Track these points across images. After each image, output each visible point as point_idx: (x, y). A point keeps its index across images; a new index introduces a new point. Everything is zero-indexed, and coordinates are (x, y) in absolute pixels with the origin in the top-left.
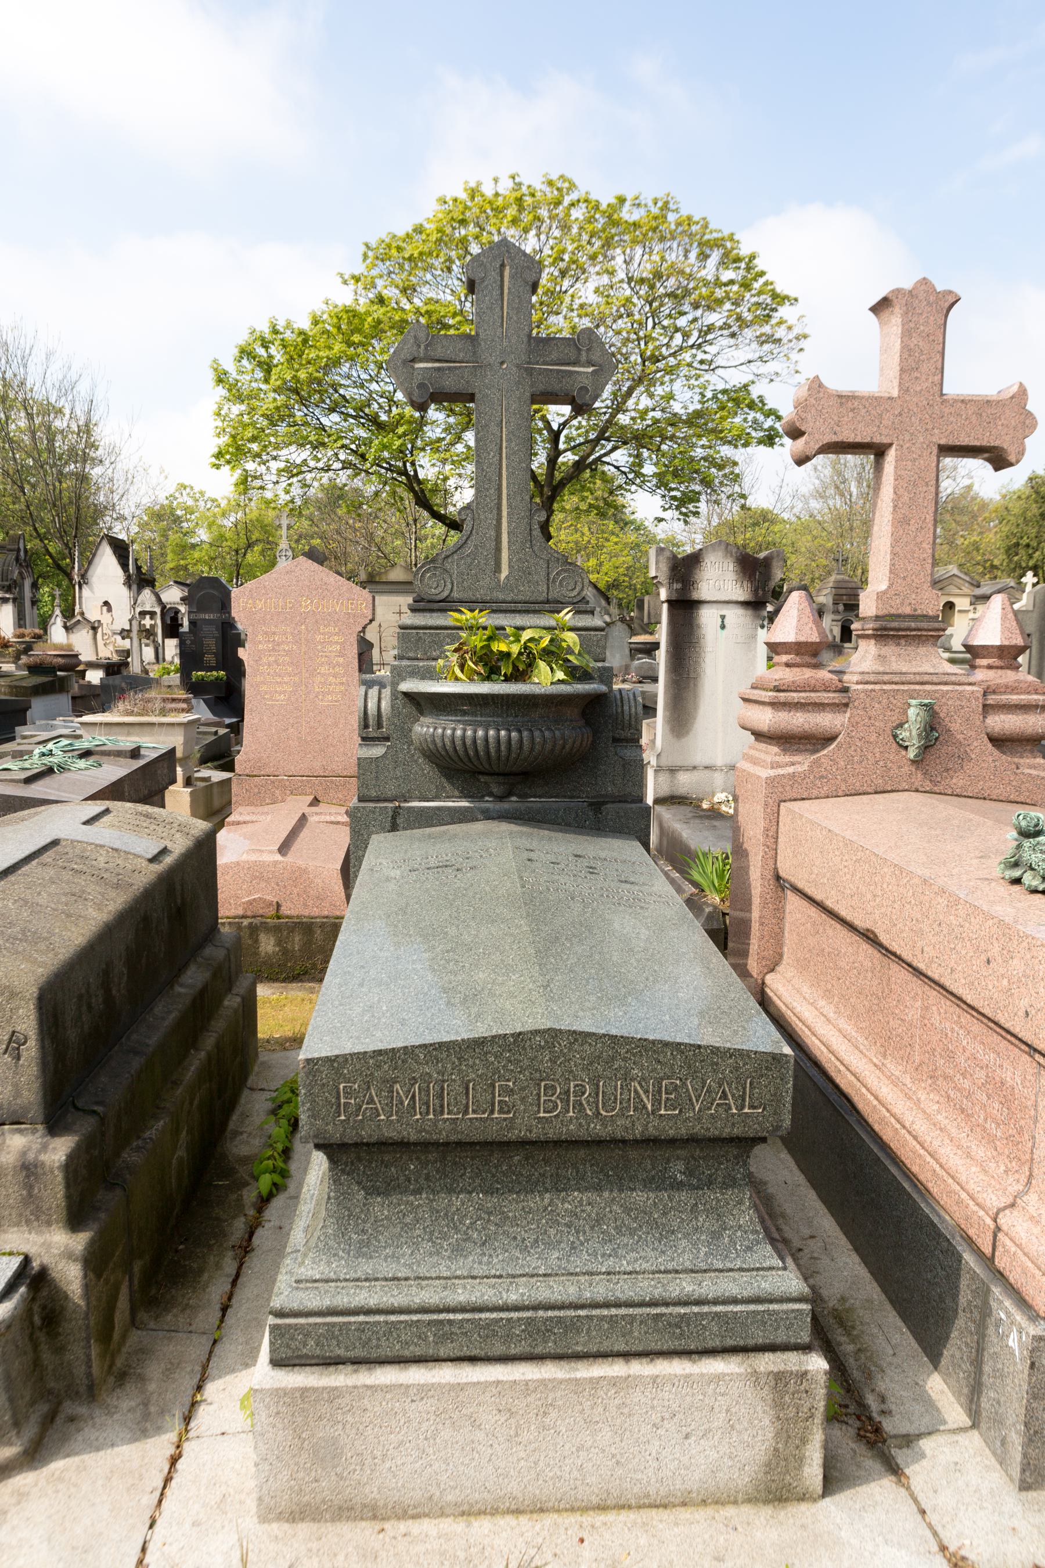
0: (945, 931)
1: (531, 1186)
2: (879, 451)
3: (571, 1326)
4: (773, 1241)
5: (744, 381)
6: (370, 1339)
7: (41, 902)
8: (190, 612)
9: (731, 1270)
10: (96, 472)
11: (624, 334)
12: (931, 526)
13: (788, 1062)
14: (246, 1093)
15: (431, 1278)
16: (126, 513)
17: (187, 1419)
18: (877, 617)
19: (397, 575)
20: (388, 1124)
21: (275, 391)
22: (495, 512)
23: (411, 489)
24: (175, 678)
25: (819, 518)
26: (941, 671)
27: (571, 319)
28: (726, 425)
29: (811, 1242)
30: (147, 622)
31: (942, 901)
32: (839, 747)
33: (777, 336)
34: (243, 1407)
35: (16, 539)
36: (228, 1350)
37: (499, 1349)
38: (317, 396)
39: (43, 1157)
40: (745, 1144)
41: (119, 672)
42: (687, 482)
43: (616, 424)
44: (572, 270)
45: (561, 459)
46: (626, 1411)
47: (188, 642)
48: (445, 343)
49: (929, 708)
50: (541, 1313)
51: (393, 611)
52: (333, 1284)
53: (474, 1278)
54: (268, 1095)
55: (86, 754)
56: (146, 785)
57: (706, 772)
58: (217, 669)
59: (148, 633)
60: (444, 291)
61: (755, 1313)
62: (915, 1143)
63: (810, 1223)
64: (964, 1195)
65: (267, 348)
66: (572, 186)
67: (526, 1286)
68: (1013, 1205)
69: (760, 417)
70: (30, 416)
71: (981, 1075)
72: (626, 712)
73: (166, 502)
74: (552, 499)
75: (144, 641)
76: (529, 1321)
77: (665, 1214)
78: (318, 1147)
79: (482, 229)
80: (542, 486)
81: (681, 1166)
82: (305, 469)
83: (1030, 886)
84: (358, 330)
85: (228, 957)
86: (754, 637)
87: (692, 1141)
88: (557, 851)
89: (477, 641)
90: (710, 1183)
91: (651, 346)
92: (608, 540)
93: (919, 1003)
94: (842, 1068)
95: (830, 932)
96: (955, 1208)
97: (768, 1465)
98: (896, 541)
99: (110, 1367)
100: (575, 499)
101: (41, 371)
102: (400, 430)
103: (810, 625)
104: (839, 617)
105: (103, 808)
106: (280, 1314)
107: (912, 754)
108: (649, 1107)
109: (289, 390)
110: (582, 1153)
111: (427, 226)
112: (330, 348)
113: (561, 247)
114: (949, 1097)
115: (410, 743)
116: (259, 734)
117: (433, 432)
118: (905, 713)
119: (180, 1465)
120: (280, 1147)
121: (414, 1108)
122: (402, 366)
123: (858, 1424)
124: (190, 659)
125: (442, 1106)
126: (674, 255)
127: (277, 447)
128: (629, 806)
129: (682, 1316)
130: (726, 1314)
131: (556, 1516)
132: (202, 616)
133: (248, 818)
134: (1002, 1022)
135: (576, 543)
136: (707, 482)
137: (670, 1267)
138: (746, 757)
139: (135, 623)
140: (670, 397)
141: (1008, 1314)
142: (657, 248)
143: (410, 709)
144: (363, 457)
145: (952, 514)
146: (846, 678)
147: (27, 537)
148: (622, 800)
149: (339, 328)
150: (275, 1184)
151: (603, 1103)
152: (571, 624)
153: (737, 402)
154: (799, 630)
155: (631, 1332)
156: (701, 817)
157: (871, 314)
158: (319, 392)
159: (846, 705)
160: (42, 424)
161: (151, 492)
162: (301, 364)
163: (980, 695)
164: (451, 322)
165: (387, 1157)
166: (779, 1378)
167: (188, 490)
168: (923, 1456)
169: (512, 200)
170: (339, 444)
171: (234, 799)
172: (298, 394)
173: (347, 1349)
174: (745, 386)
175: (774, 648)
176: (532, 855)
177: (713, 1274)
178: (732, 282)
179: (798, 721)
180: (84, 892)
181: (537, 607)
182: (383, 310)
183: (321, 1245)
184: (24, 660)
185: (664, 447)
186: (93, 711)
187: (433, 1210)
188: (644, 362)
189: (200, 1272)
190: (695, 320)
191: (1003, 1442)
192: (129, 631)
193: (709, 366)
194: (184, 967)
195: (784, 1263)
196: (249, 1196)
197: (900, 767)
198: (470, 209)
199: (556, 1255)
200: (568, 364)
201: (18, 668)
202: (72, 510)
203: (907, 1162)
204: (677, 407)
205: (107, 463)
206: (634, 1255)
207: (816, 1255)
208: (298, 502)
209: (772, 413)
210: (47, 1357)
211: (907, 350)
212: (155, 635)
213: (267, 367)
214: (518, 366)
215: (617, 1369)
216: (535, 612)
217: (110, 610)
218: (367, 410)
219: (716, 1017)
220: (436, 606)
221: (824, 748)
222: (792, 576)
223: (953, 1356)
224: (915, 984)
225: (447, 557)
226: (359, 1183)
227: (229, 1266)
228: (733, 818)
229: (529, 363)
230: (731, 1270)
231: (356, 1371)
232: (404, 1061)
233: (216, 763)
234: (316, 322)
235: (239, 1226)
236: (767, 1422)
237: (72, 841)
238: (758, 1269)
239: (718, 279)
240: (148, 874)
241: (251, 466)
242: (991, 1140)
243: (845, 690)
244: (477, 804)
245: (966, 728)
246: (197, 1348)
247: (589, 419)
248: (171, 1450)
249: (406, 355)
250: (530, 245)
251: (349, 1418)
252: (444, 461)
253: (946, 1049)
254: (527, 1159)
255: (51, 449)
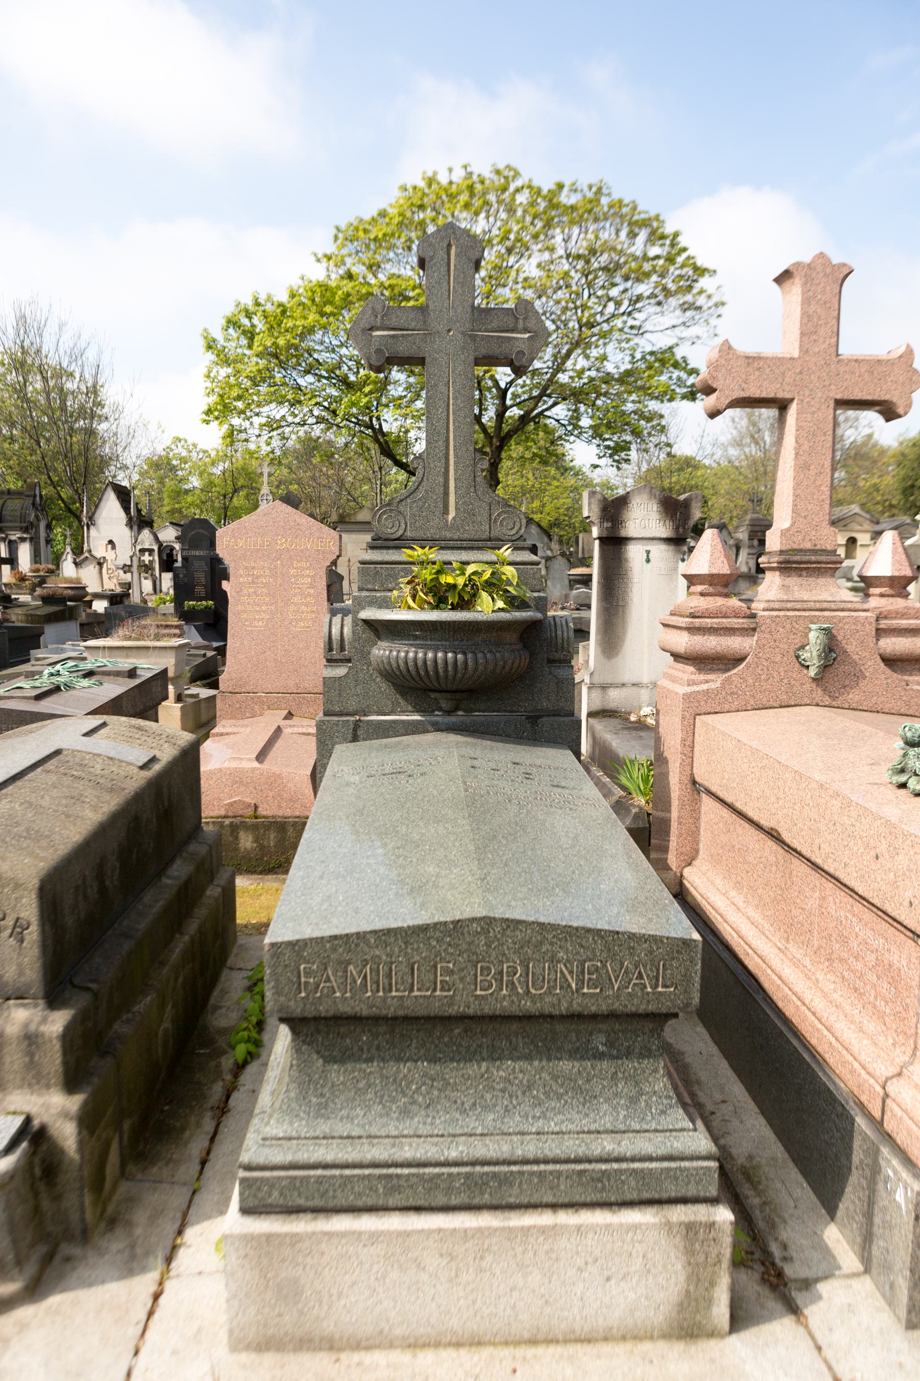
0: (839, 830)
1: (470, 1056)
2: (782, 406)
3: (505, 1180)
4: (684, 1106)
5: (669, 344)
6: (327, 1191)
7: (44, 804)
8: (182, 550)
9: (647, 1131)
10: (102, 427)
11: (563, 303)
12: (828, 471)
13: (696, 946)
14: (226, 972)
15: (380, 1137)
16: (128, 462)
17: (169, 1260)
18: (781, 551)
19: (364, 516)
20: (343, 1001)
21: (257, 356)
22: (443, 461)
23: (377, 441)
24: (170, 607)
25: (737, 464)
26: (838, 599)
27: (516, 291)
28: (654, 382)
29: (723, 1106)
30: (146, 558)
31: (837, 803)
32: (748, 667)
33: (698, 304)
34: (217, 1249)
35: (33, 486)
36: (205, 1199)
37: (441, 1200)
38: (294, 360)
39: (43, 1028)
40: (660, 1018)
41: (121, 602)
42: (619, 432)
43: (557, 382)
44: (517, 248)
45: (508, 414)
46: (554, 1256)
47: (181, 576)
48: (399, 313)
49: (828, 632)
50: (478, 1169)
51: (356, 547)
52: (295, 1142)
53: (419, 1136)
54: (245, 974)
55: (89, 674)
56: (141, 701)
57: (634, 688)
58: (206, 599)
59: (147, 568)
60: (403, 268)
61: (669, 1170)
62: (813, 1018)
63: (722, 1089)
64: (856, 1065)
65: (250, 318)
66: (517, 174)
67: (465, 1144)
68: (899, 1074)
69: (683, 375)
70: (45, 379)
71: (871, 958)
72: (560, 636)
73: (164, 453)
74: (500, 448)
75: (143, 575)
76: (468, 1176)
77: (588, 1081)
78: (282, 1020)
79: (438, 213)
80: (491, 438)
81: (602, 1038)
82: (284, 423)
83: (914, 790)
84: (331, 303)
85: (210, 852)
86: (676, 569)
87: (612, 1016)
88: (497, 758)
89: (427, 574)
90: (628, 1054)
91: (586, 314)
92: (549, 484)
93: (817, 894)
94: (750, 951)
95: (740, 831)
96: (849, 1076)
97: (681, 1304)
98: (797, 485)
99: (103, 1213)
100: (521, 449)
101: (54, 340)
102: (367, 389)
103: (722, 558)
104: (754, 551)
105: (100, 722)
106: (248, 1168)
107: (812, 672)
108: (574, 986)
109: (269, 354)
110: (515, 1026)
111: (390, 210)
112: (305, 318)
113: (508, 227)
114: (843, 977)
115: (369, 664)
116: (241, 656)
117: (396, 391)
118: (806, 636)
119: (162, 1300)
120: (254, 1020)
121: (366, 985)
122: (361, 332)
123: (762, 1269)
124: (182, 591)
125: (390, 985)
126: (606, 235)
127: (259, 405)
128: (562, 719)
129: (603, 1172)
130: (642, 1170)
131: (491, 1349)
132: (193, 553)
133: (230, 730)
134: (889, 911)
135: (522, 487)
136: (636, 433)
137: (593, 1127)
138: (666, 676)
139: (135, 559)
140: (604, 358)
141: (895, 1172)
142: (592, 227)
143: (368, 634)
144: (334, 412)
145: (855, 459)
146: (754, 605)
147: (42, 484)
148: (556, 714)
149: (313, 300)
150: (249, 1053)
151: (533, 983)
152: (511, 559)
153: (663, 362)
154: (712, 563)
155: (558, 1185)
156: (629, 728)
157: (775, 285)
158: (296, 356)
159: (754, 630)
160: (55, 386)
161: (150, 445)
162: (280, 332)
163: (873, 620)
164: (411, 294)
165: (342, 1030)
166: (690, 1228)
167: (183, 442)
168: (820, 1297)
169: (464, 187)
170: (313, 401)
171: (218, 714)
172: (277, 358)
173: (307, 1199)
174: (671, 348)
175: (692, 580)
176: (475, 763)
177: (631, 1135)
178: (657, 257)
179: (711, 644)
180: (82, 795)
181: (480, 544)
182: (351, 284)
183: (285, 1107)
184: (39, 591)
185: (599, 402)
186: (96, 636)
187: (382, 1076)
188: (581, 328)
189: (183, 1129)
190: (625, 291)
191: (892, 1286)
192: (130, 566)
193: (638, 330)
194: (172, 860)
195: (694, 1124)
196: (227, 1063)
197: (802, 684)
198: (428, 195)
199: (491, 1117)
200: (507, 331)
201: (34, 599)
202: (81, 461)
203: (807, 1035)
204: (610, 367)
205: (112, 419)
206: (561, 1117)
207: (727, 1118)
208: (278, 453)
209: (694, 372)
210: (46, 1204)
211: (806, 317)
212: (153, 569)
213: (250, 335)
214: (463, 333)
215: (545, 1218)
216: (479, 548)
217: (114, 547)
218: (338, 372)
219: (634, 906)
220: (391, 543)
221: (734, 668)
222: (712, 514)
223: (847, 1209)
224: (814, 876)
225: (401, 501)
226: (318, 1052)
227: (208, 1125)
228: (655, 729)
229: (472, 330)
230: (647, 1131)
231: (315, 1219)
232: (357, 945)
233: (204, 682)
234: (293, 296)
235: (217, 1090)
236: (679, 1266)
237: (73, 751)
238: (671, 1131)
239: (645, 254)
240: (138, 780)
241: (236, 421)
242: (881, 1016)
243: (753, 616)
244: (428, 718)
245: (860, 649)
246: (179, 1197)
247: (532, 379)
248: (153, 1288)
249: (364, 324)
250: (480, 226)
251: (309, 1259)
252: (405, 416)
253: (841, 935)
254: (466, 1031)
255: (63, 408)
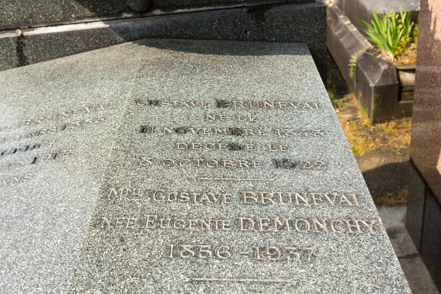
244: (114, 24)
